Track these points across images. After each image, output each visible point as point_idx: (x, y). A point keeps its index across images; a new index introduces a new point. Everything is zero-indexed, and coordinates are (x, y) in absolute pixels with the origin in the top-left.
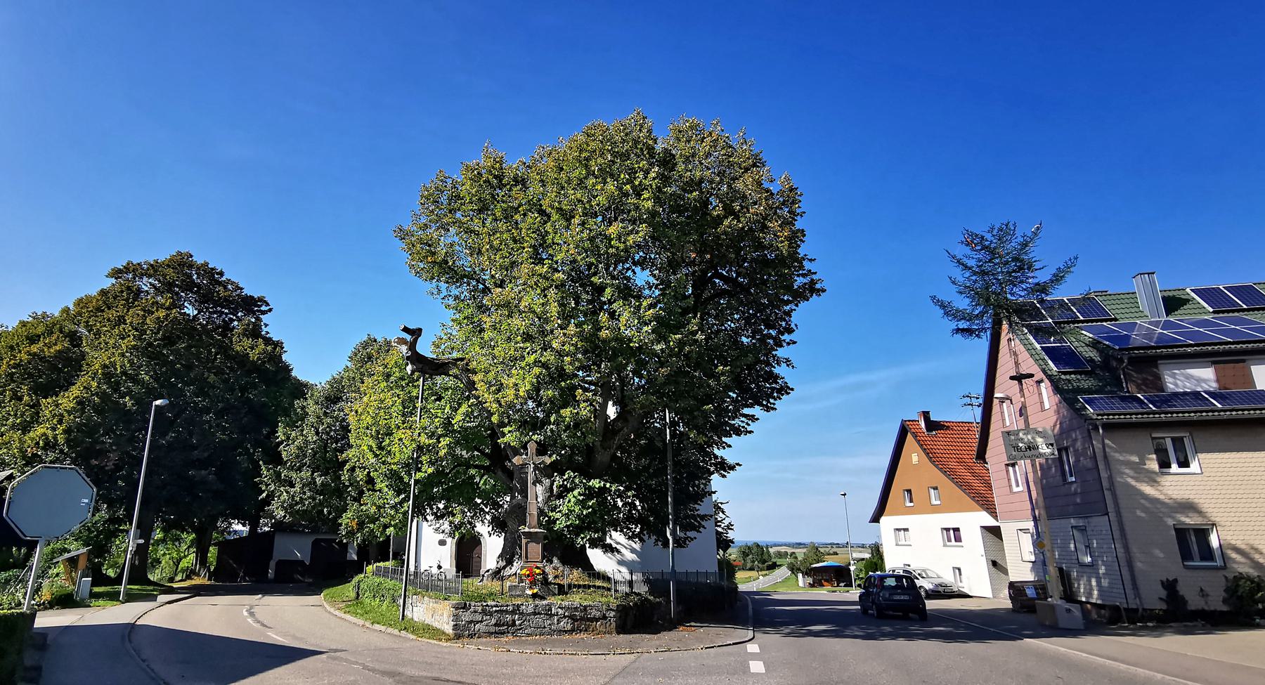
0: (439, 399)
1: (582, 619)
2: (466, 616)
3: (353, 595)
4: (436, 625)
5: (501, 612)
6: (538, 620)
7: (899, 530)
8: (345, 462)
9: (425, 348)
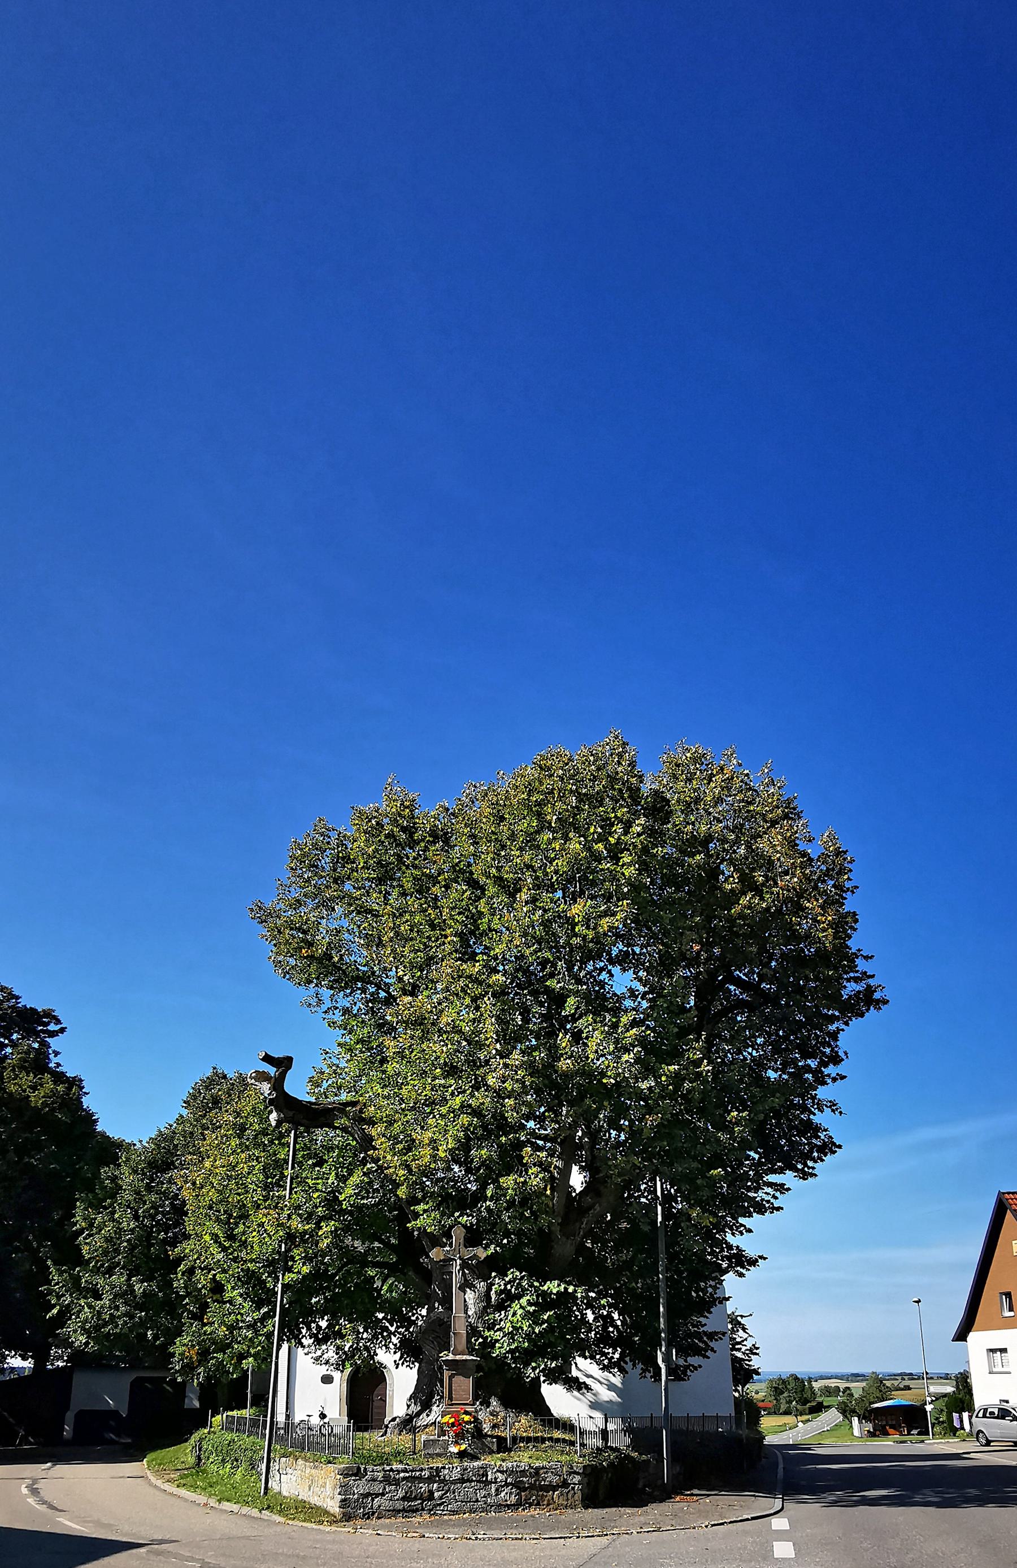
0: (321, 1163)
1: (532, 1487)
2: (360, 1487)
3: (191, 1460)
4: (315, 1500)
6: (468, 1489)
7: (993, 1351)
8: (179, 1261)
9: (298, 1087)
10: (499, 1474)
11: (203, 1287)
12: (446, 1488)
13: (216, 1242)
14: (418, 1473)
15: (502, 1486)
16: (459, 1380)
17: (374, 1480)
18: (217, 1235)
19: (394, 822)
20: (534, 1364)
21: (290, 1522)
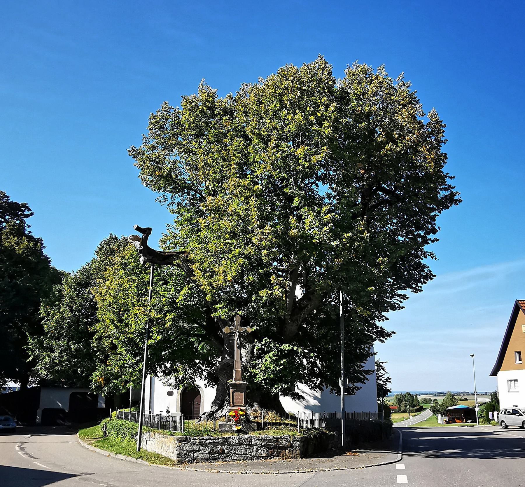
0: (166, 283)
1: (275, 447)
2: (187, 447)
3: (101, 434)
4: (164, 454)
5: (213, 443)
6: (242, 449)
7: (511, 381)
8: (94, 333)
9: (154, 243)
10: (258, 441)
11: (106, 346)
12: (231, 448)
13: (113, 323)
14: (216, 441)
16: (237, 394)
17: (194, 444)
18: (113, 320)
19: (204, 105)
20: (276, 386)
21: (152, 465)
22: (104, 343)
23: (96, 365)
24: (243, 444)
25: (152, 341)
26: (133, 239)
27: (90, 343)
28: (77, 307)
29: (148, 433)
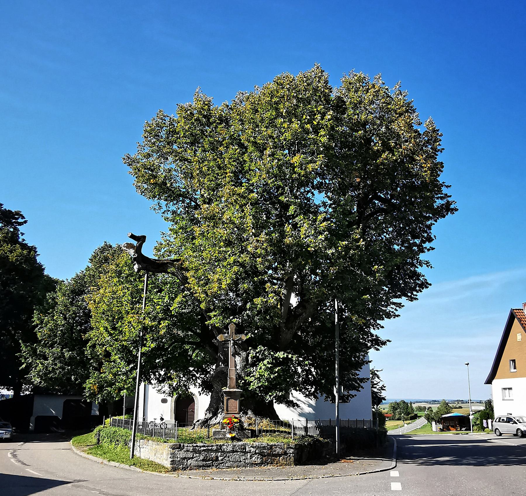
0: (160, 291)
1: (269, 455)
2: (181, 454)
3: (95, 441)
4: (157, 461)
5: (207, 451)
6: (236, 456)
7: (505, 389)
8: (88, 340)
9: (149, 251)
10: (252, 448)
11: (100, 354)
12: (225, 455)
13: (106, 331)
14: (210, 448)
15: (253, 454)
16: (232, 401)
17: (188, 451)
18: (107, 328)
19: (200, 113)
20: (270, 394)
22: (98, 351)
23: (90, 373)
24: (237, 452)
25: (146, 348)
26: (127, 247)
27: (84, 350)
28: (71, 315)
29: (141, 441)
